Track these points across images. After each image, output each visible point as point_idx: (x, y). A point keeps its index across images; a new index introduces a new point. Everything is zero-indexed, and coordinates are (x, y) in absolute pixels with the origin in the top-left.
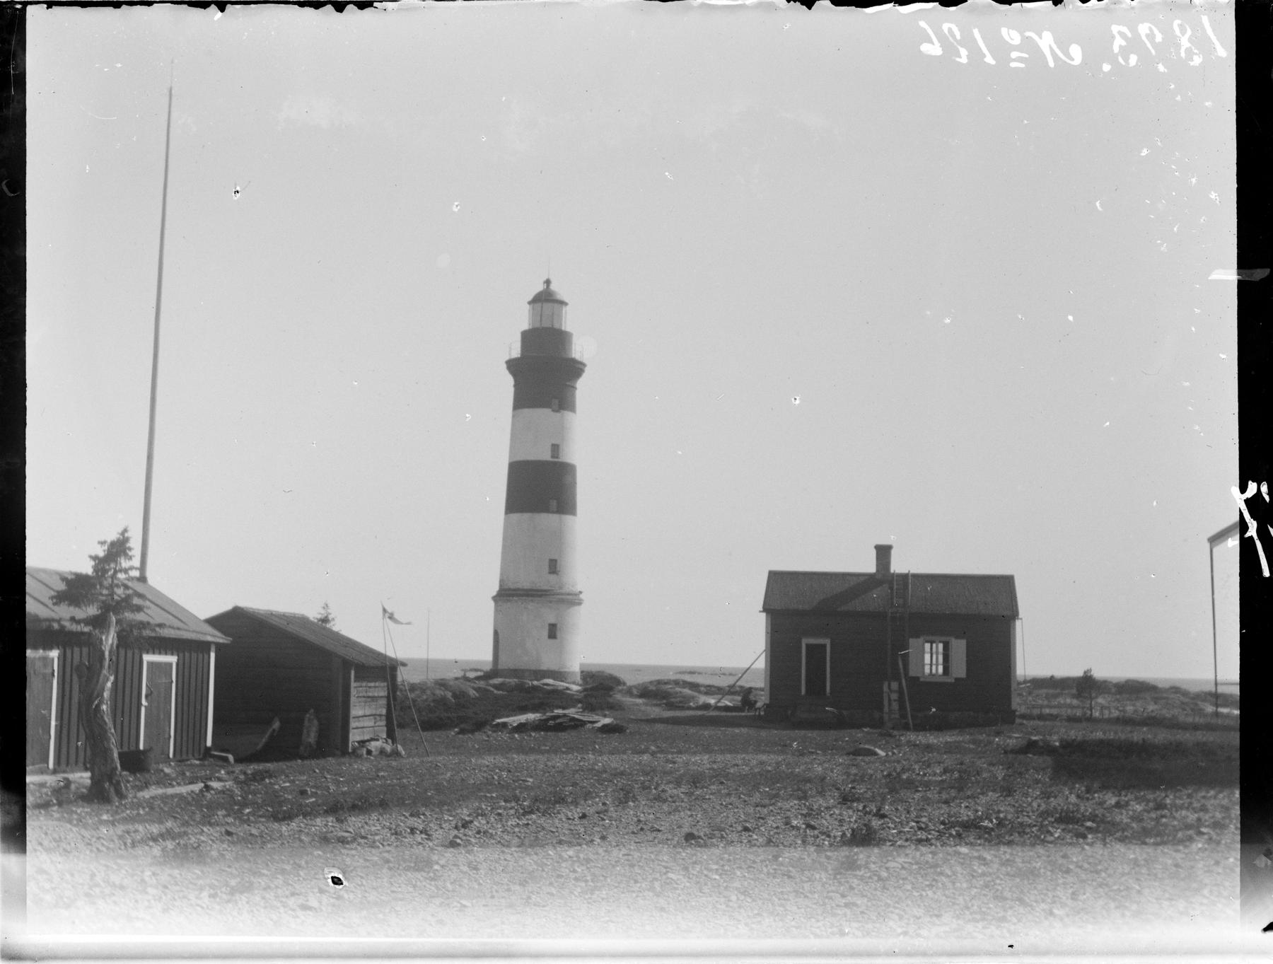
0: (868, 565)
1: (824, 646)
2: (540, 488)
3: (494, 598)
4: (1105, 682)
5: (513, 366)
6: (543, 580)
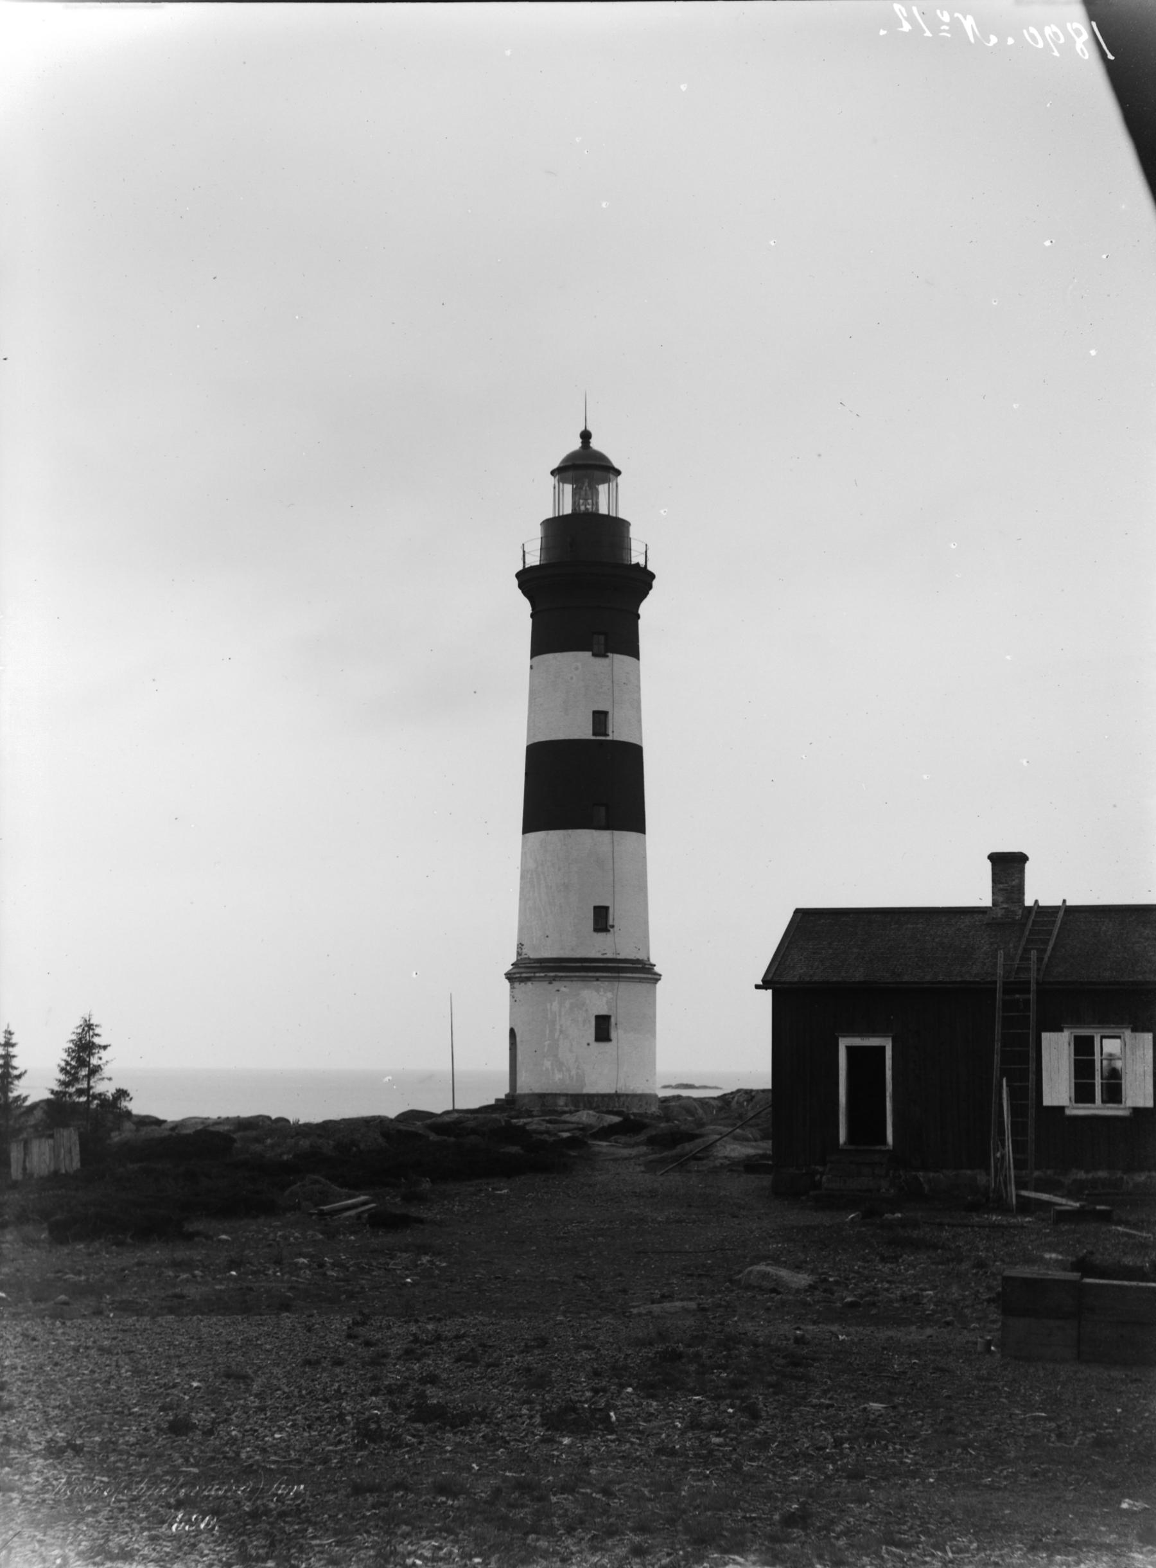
0: (975, 890)
1: (883, 1048)
2: (585, 785)
3: (510, 977)
4: (183, 1120)
5: (528, 580)
6: (598, 947)
